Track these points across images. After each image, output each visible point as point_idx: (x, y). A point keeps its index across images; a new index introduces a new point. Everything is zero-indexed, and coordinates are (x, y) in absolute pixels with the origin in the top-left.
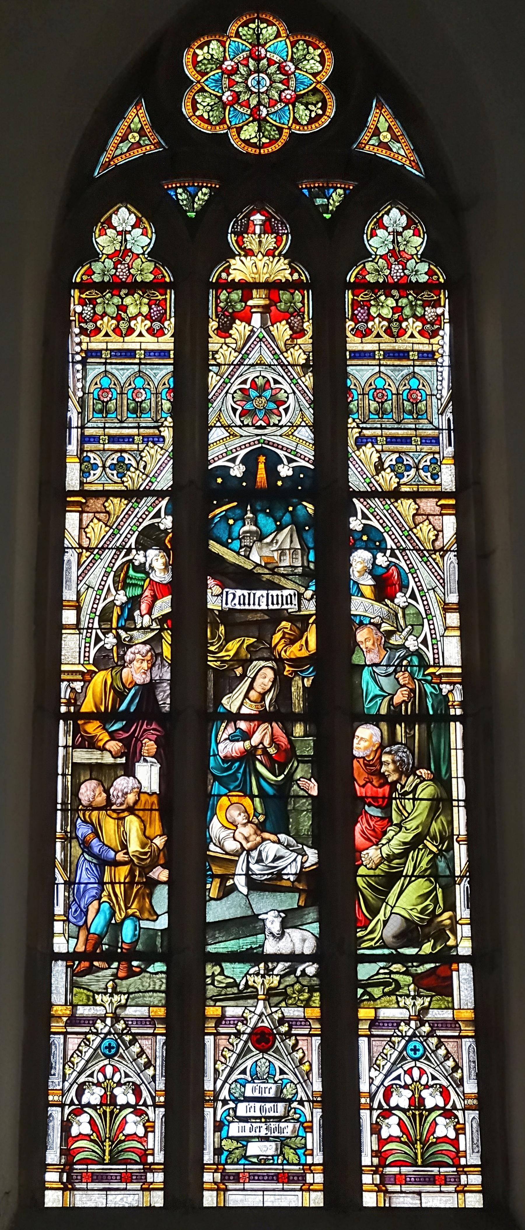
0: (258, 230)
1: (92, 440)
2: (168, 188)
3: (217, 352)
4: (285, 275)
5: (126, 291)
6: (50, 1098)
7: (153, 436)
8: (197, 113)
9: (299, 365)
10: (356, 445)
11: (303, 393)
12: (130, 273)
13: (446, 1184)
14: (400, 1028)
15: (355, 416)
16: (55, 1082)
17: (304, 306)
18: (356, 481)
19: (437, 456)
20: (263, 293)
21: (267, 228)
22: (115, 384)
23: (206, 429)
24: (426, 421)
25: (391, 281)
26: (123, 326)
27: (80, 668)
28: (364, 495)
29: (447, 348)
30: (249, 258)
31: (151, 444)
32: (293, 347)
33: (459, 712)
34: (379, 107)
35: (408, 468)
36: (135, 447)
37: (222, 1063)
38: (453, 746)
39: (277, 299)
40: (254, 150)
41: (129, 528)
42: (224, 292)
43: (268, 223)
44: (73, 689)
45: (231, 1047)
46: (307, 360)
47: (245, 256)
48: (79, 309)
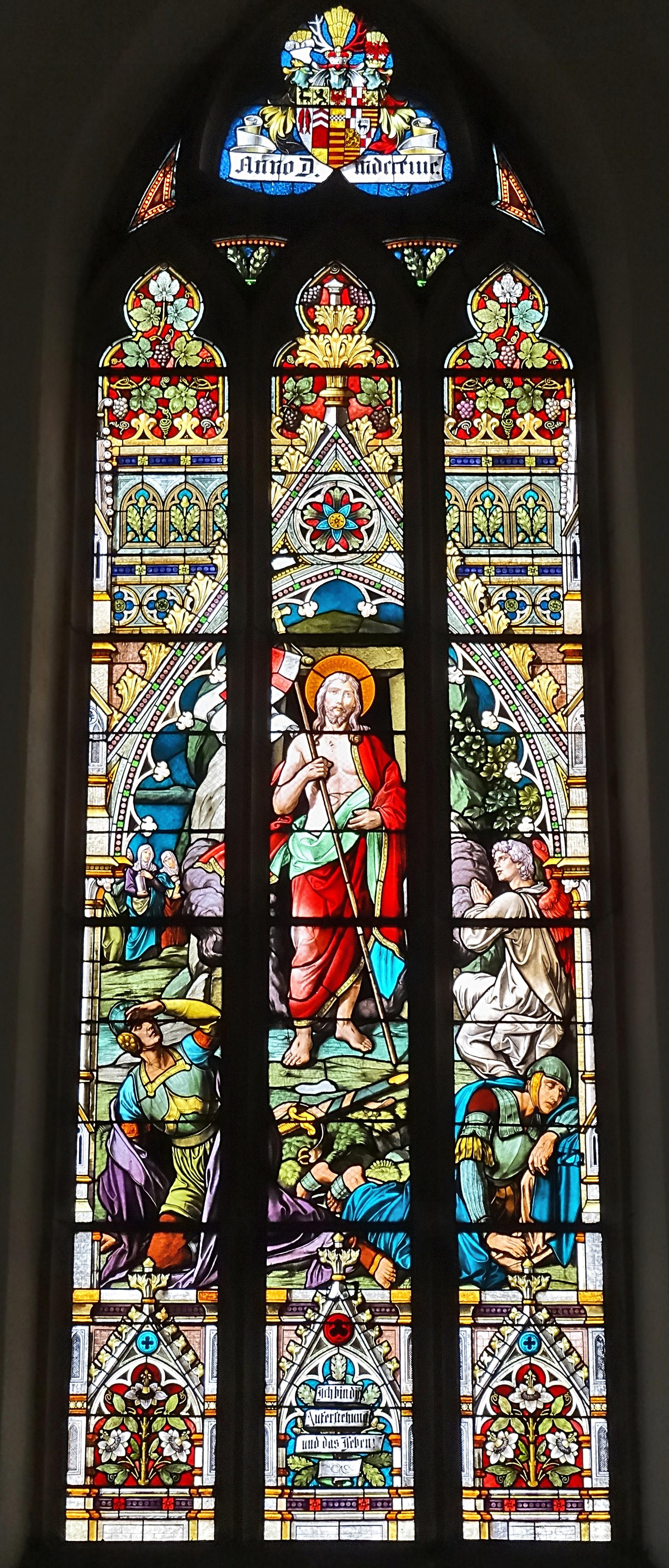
0: (333, 299)
1: (552, 571)
2: (393, 249)
3: (282, 457)
4: (364, 360)
6: (72, 1405)
7: (203, 566)
10: (457, 576)
12: (517, 357)
13: (175, 1510)
16: (77, 1387)
17: (391, 397)
18: (457, 623)
19: (558, 590)
20: (339, 382)
21: (345, 298)
26: (164, 425)
27: (110, 861)
28: (464, 639)
29: (573, 450)
30: (321, 336)
31: (199, 575)
33: (585, 915)
35: (522, 605)
36: (180, 578)
37: (288, 1360)
41: (172, 682)
42: (291, 379)
43: (346, 290)
46: (395, 465)
47: (317, 334)
48: (108, 402)
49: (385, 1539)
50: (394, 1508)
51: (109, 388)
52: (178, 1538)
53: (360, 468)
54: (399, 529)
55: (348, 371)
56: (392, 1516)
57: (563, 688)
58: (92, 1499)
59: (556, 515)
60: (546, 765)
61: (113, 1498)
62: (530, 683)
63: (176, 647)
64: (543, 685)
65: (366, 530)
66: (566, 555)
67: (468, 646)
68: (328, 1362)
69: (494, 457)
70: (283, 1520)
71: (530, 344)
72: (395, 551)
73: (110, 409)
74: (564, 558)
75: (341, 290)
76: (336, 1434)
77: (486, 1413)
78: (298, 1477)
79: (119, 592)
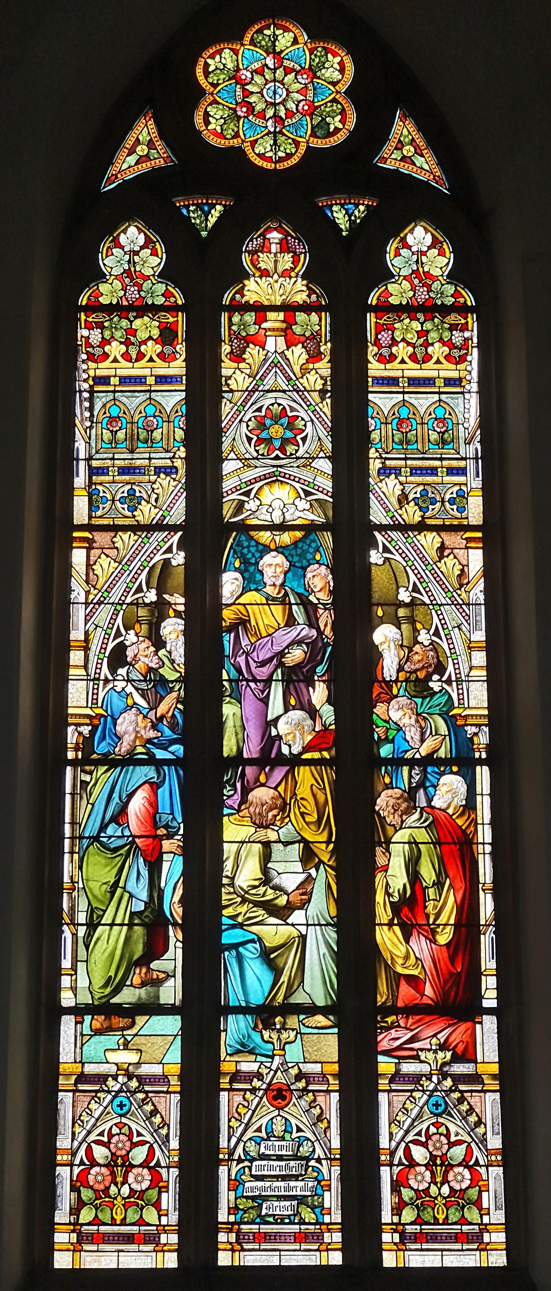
3: (230, 378)
4: (301, 298)
5: (135, 314)
6: (59, 1158)
7: (166, 468)
8: (341, 126)
9: (315, 391)
11: (322, 422)
14: (108, 1083)
15: (379, 446)
16: (63, 1142)
18: (377, 515)
21: (284, 247)
22: (414, 414)
23: (220, 460)
24: (453, 451)
25: (125, 303)
28: (382, 528)
29: (475, 374)
30: (264, 279)
31: (162, 476)
32: (309, 373)
34: (403, 118)
38: (478, 790)
39: (291, 322)
40: (269, 165)
41: (140, 563)
42: (237, 313)
44: (80, 733)
45: (246, 1104)
47: (261, 277)
49: (478, 1265)
50: (325, 1241)
51: (86, 320)
52: (472, 1264)
53: (295, 387)
54: (329, 437)
55: (289, 309)
56: (323, 1247)
57: (466, 568)
58: (75, 1234)
59: (460, 426)
60: (452, 632)
61: (416, 1233)
62: (439, 564)
63: (143, 536)
64: (450, 565)
65: (301, 439)
66: (470, 458)
67: (386, 533)
68: (270, 1122)
69: (409, 379)
70: (233, 1250)
71: (150, 285)
72: (326, 457)
73: (88, 338)
74: (468, 461)
75: (281, 240)
76: (278, 1181)
77: (82, 1163)
78: (246, 1215)
79: (96, 488)
